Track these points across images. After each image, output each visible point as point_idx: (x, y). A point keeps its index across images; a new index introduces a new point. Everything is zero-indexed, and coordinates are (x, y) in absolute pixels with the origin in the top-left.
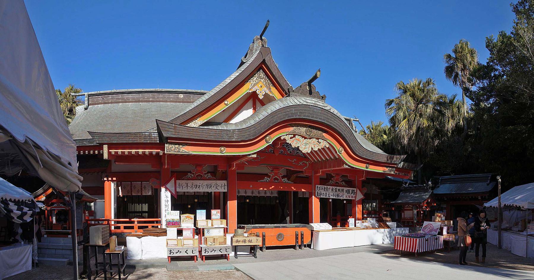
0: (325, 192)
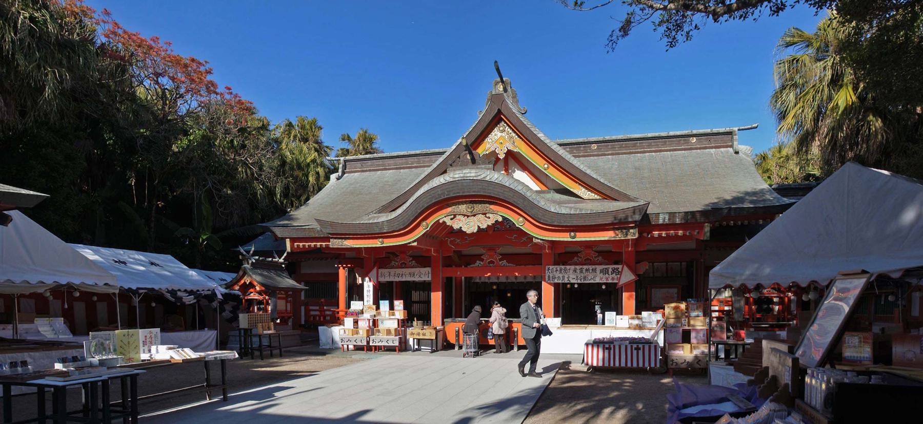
0: (561, 275)
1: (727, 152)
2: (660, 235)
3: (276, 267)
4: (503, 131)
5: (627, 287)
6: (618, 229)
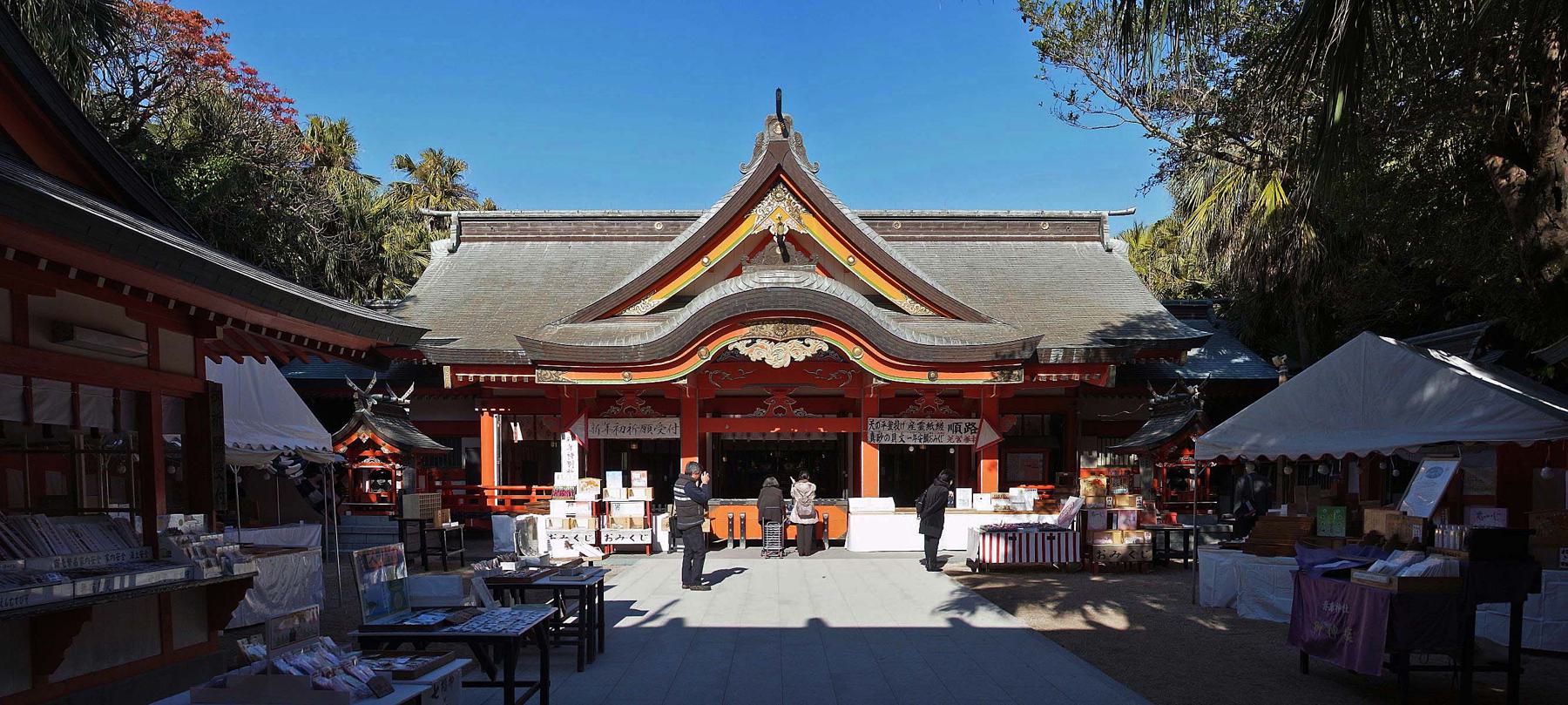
1: (1096, 249)
4: (780, 200)
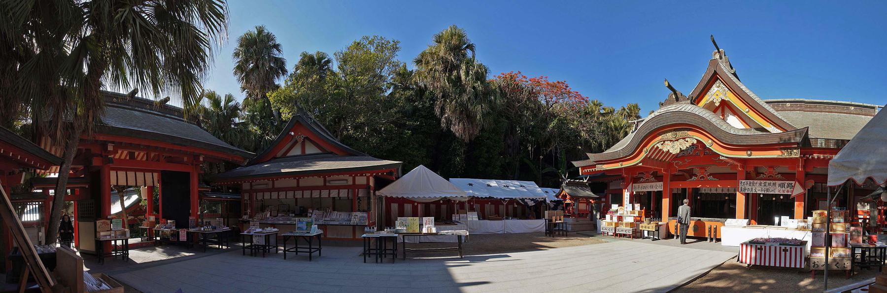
2: (819, 158)
3: (582, 185)
5: (799, 197)
6: (784, 149)
